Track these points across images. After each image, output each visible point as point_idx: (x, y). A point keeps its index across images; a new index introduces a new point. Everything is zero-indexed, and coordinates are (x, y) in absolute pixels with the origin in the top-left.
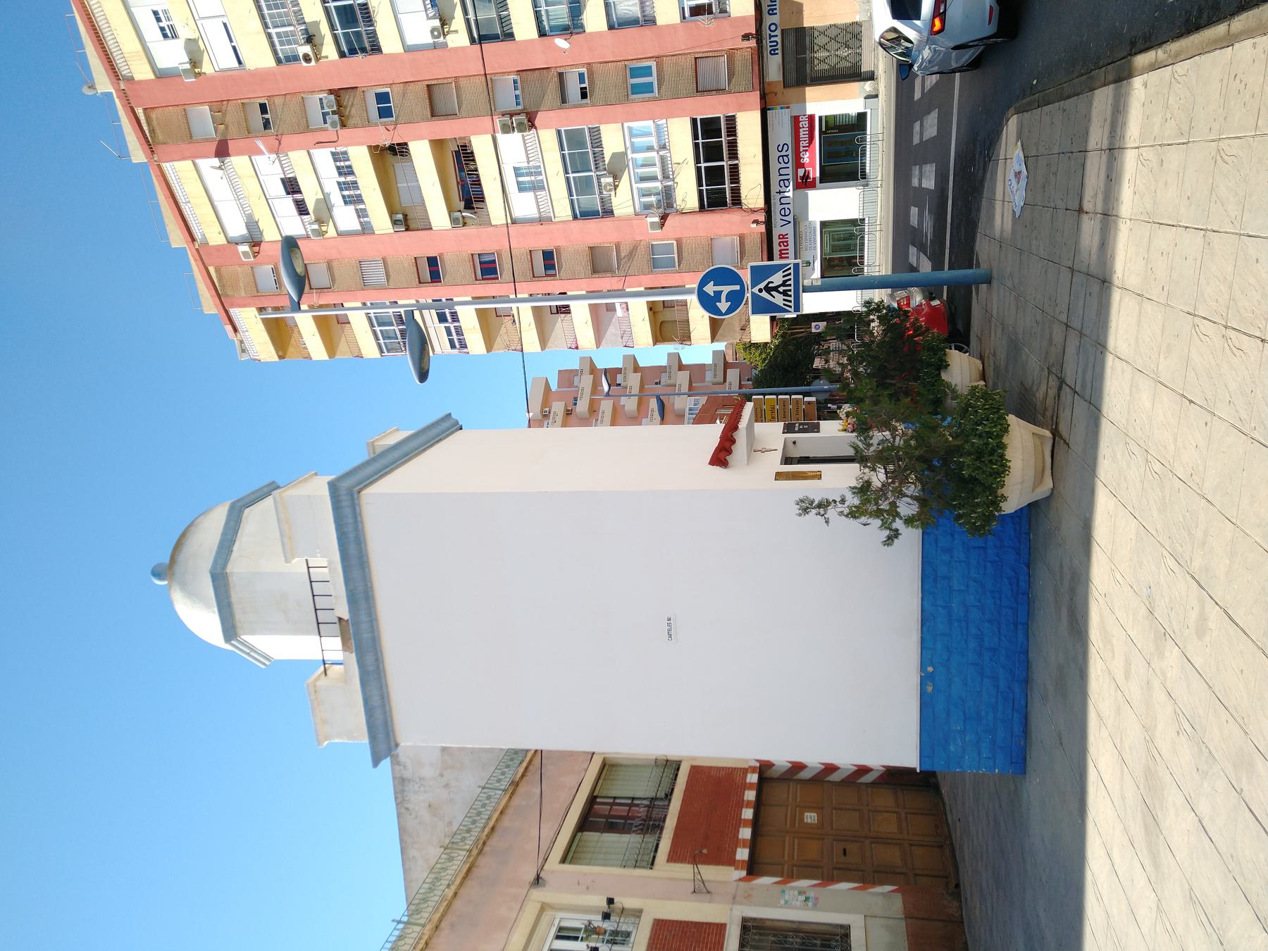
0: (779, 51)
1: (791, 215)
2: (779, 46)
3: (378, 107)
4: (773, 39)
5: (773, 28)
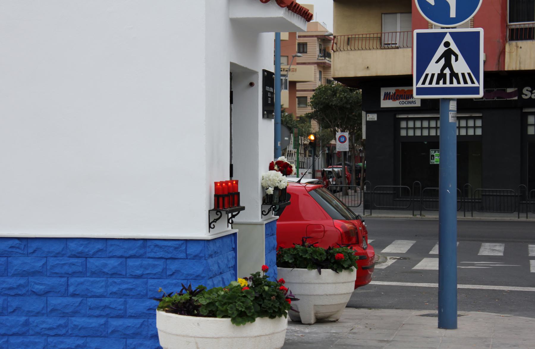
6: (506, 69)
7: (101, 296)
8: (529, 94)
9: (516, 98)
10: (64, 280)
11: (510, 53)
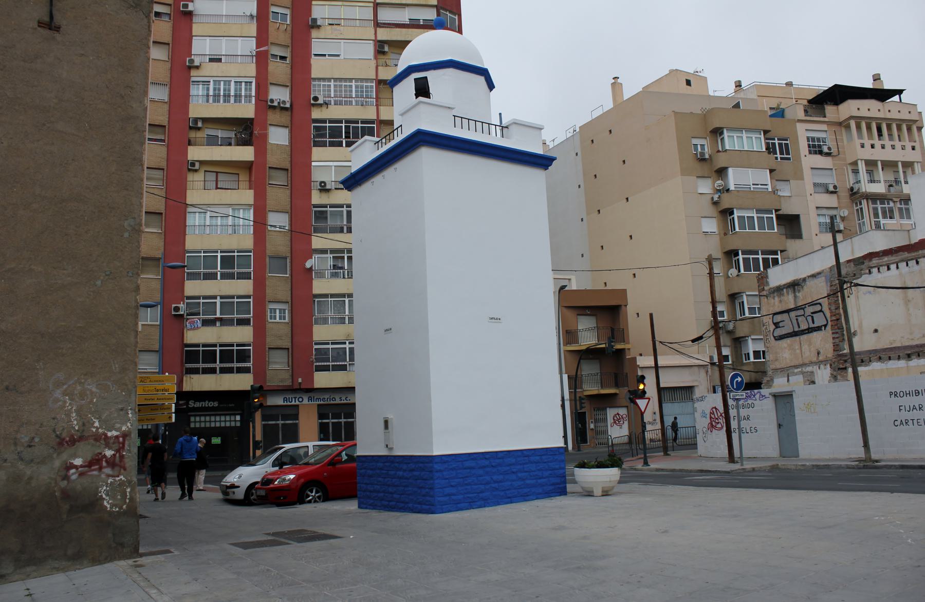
0: (285, 403)
1: (299, 403)
2: (289, 403)
3: (346, 147)
4: (294, 399)
5: (300, 400)
6: (184, 390)
7: (534, 471)
8: (193, 405)
9: (185, 407)
10: (522, 466)
11: (186, 381)
